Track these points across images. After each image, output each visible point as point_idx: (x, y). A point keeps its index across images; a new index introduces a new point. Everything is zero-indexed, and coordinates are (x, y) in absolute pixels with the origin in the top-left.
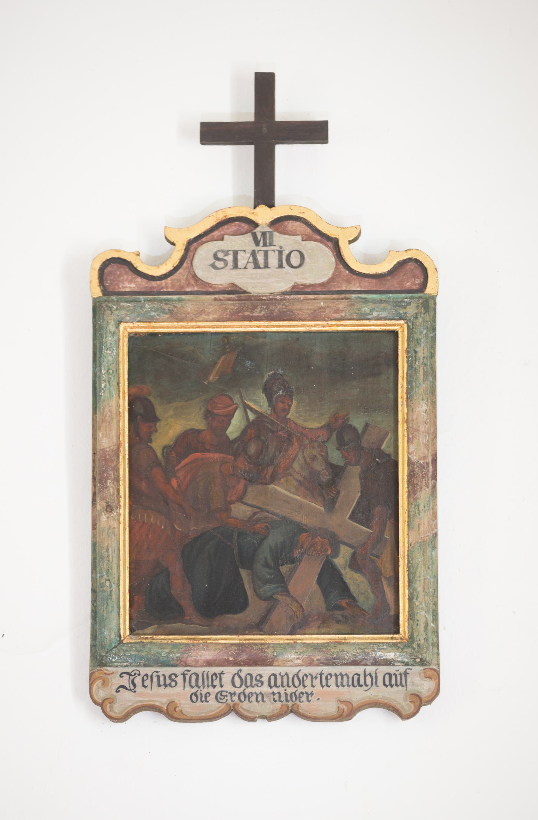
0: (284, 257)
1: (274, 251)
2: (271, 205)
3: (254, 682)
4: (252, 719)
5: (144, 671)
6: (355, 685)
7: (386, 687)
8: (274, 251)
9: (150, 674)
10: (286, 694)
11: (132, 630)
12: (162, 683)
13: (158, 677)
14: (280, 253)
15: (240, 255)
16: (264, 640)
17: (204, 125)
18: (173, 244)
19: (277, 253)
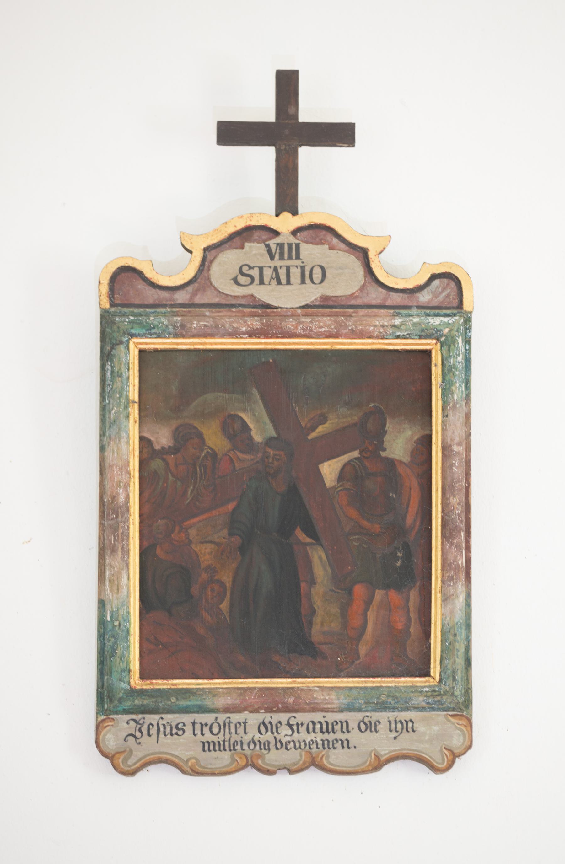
0: (307, 274)
1: (297, 267)
2: (295, 212)
8: (297, 267)
14: (303, 269)
16: (305, 683)
18: (191, 252)
19: (299, 268)
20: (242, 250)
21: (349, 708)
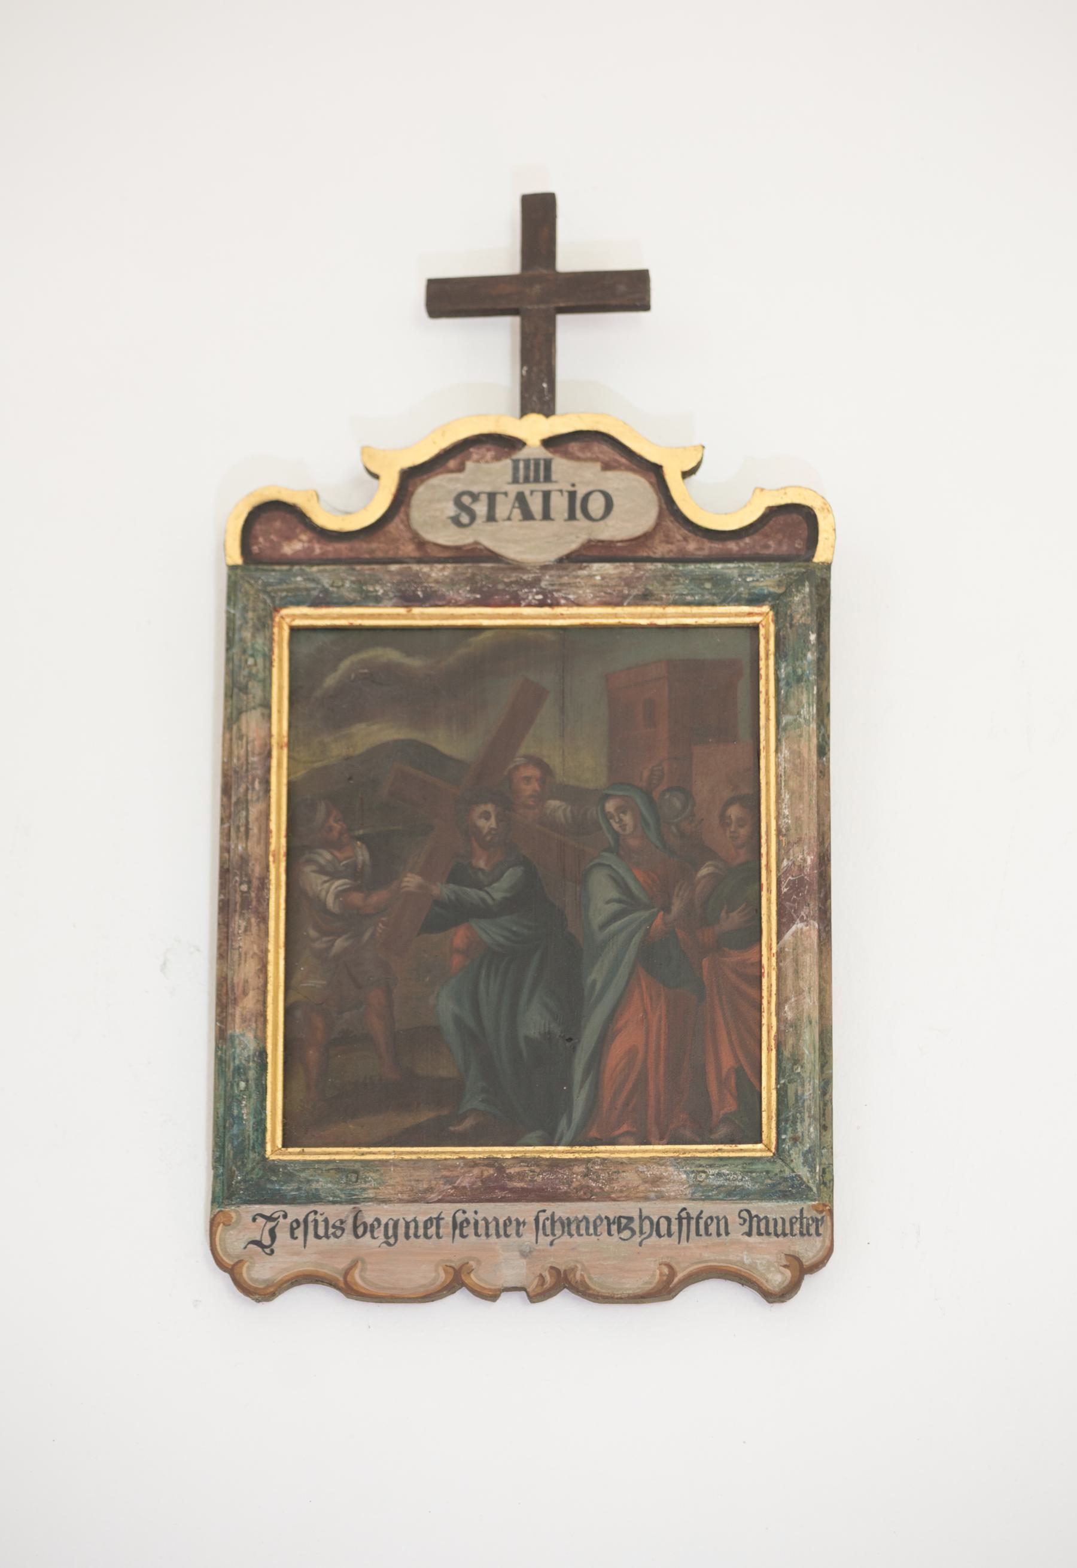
1: (561, 491)
2: (548, 409)
3: (331, 1230)
8: (561, 491)
9: (301, 1219)
13: (316, 1221)
14: (572, 495)
15: (500, 498)
18: (376, 477)
19: (566, 495)
21: (733, 1193)
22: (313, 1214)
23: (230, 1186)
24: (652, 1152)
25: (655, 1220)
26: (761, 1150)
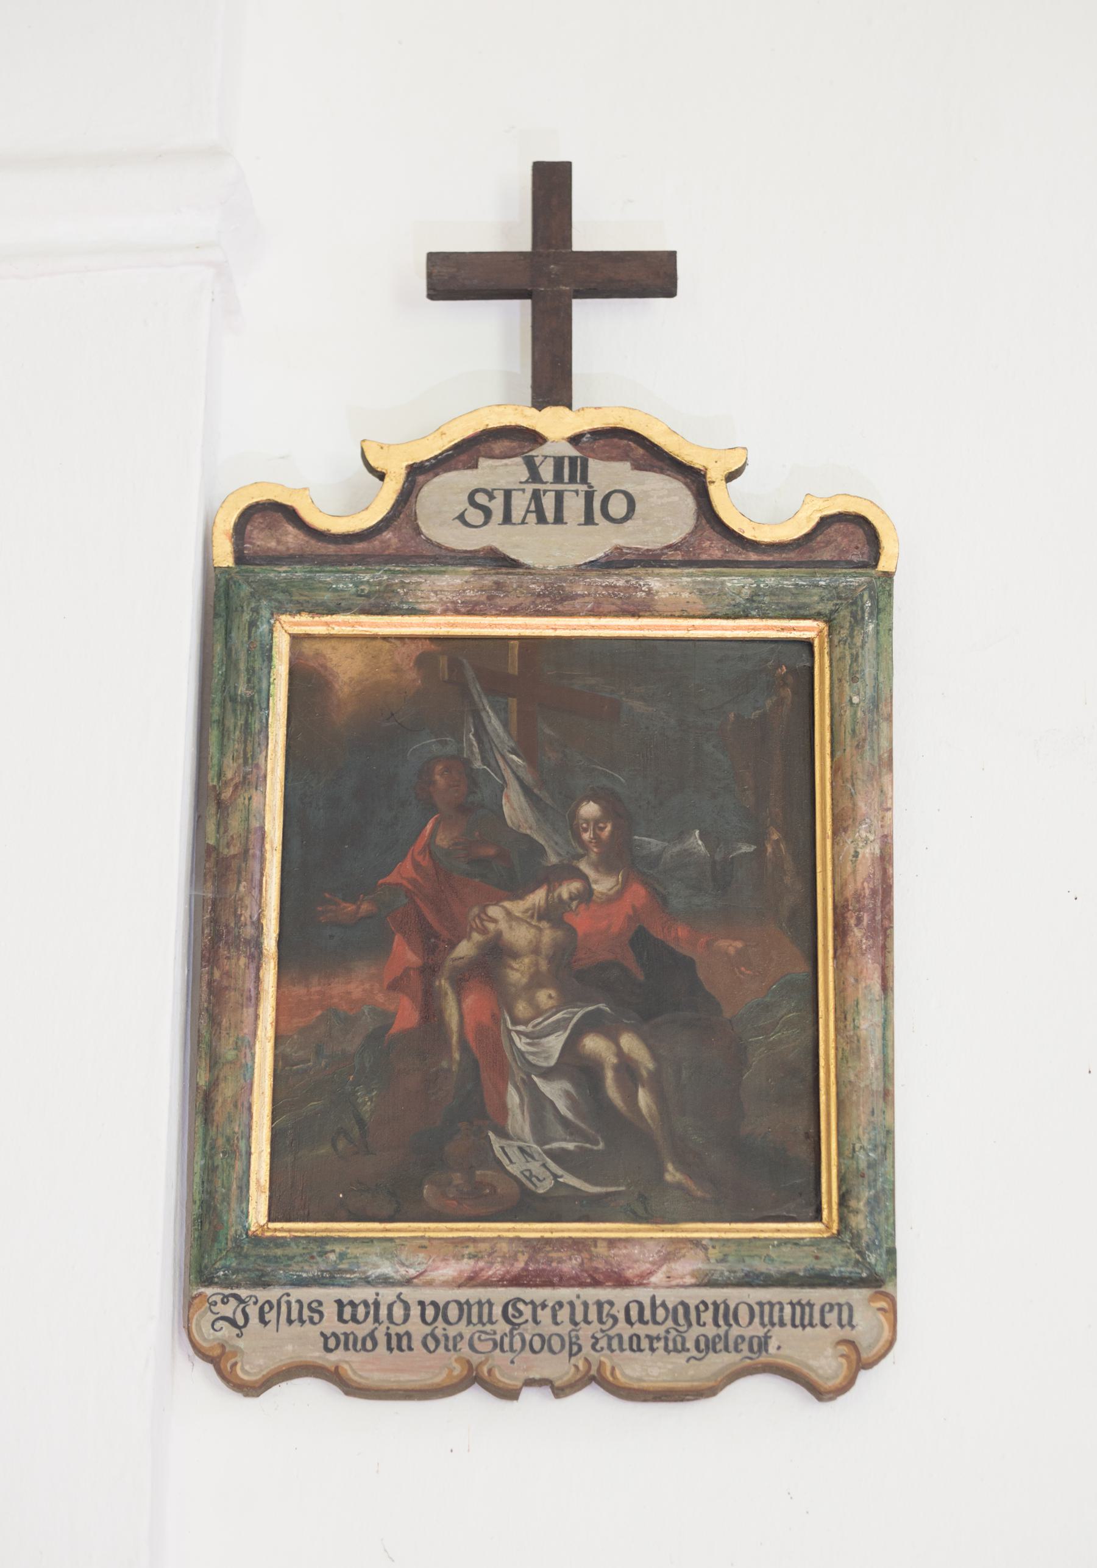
0: (597, 505)
4: (511, 1394)
5: (263, 1295)
6: (646, 1319)
7: (263, 1325)
10: (446, 1337)
11: (817, 1217)
12: (294, 1315)
13: (289, 1303)
14: (589, 497)
17: (435, 259)
18: (381, 476)
20: (475, 471)
22: (285, 1296)
23: (200, 1266)
24: (488, 1231)
25: (670, 1306)
26: (820, 1231)
